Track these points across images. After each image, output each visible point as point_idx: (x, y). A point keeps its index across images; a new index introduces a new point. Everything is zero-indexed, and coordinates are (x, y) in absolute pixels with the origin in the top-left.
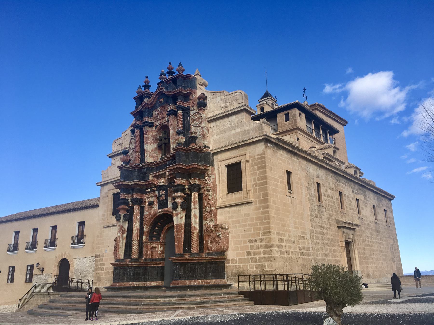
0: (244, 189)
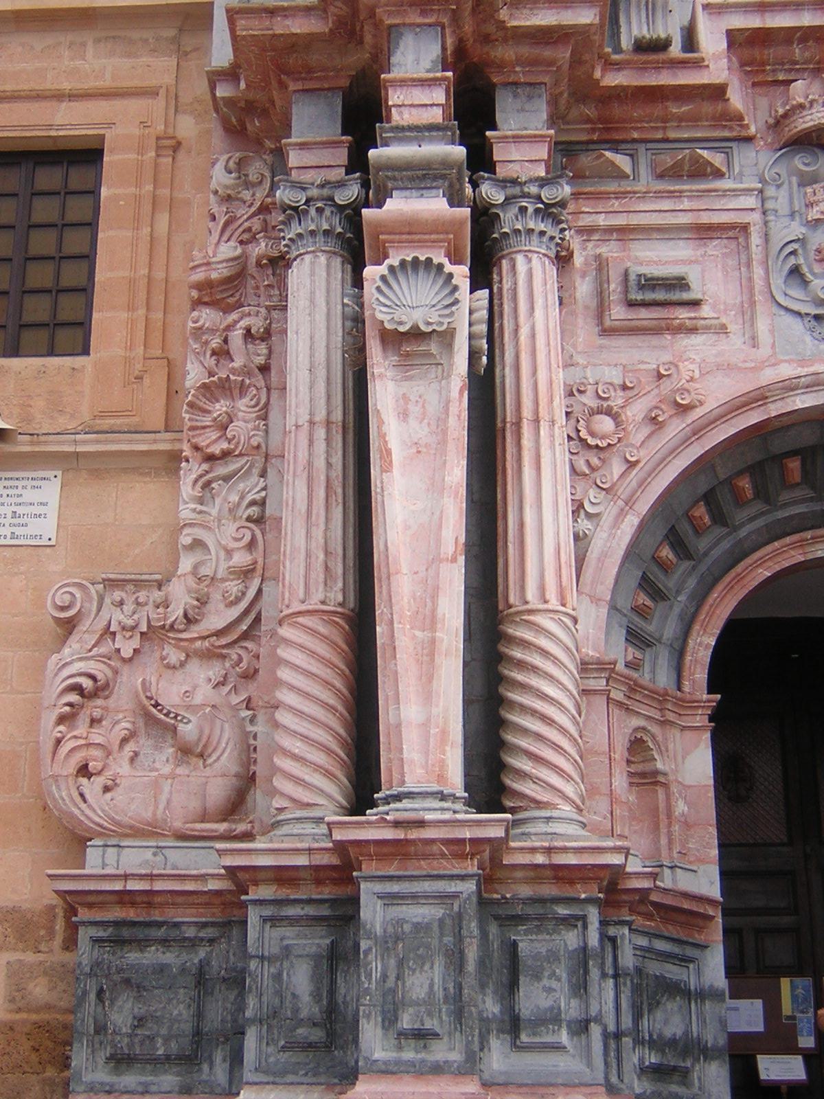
0: (110, 320)
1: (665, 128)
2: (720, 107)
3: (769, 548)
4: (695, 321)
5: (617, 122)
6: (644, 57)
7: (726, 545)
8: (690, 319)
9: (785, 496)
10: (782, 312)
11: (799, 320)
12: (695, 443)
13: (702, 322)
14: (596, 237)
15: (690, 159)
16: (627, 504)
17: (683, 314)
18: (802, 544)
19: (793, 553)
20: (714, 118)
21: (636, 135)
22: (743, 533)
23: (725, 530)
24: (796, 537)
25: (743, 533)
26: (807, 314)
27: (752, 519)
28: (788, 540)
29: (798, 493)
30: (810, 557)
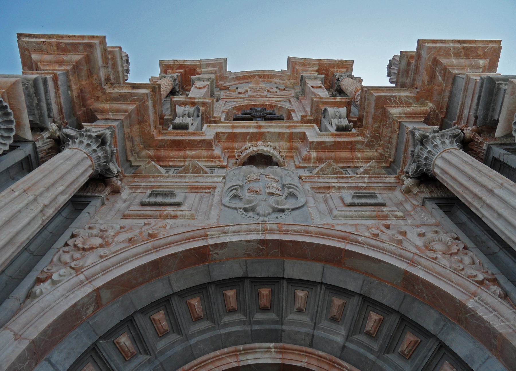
1: (185, 161)
2: (210, 152)
3: (212, 355)
4: (176, 212)
5: (163, 158)
6: (176, 131)
7: (178, 348)
8: (173, 211)
9: (226, 319)
10: (227, 209)
11: (235, 211)
12: (154, 254)
13: (181, 213)
14: (139, 191)
15: (192, 166)
16: (87, 279)
17: (170, 210)
18: (236, 353)
19: (229, 360)
20: (207, 157)
21: (171, 164)
22: (193, 341)
23: (179, 337)
24: (232, 349)
25: (193, 341)
26: (240, 208)
27: (203, 332)
28: (226, 350)
29: (235, 317)
30: (242, 364)
